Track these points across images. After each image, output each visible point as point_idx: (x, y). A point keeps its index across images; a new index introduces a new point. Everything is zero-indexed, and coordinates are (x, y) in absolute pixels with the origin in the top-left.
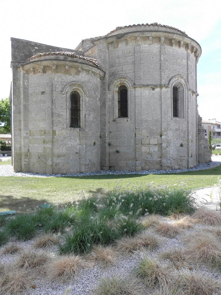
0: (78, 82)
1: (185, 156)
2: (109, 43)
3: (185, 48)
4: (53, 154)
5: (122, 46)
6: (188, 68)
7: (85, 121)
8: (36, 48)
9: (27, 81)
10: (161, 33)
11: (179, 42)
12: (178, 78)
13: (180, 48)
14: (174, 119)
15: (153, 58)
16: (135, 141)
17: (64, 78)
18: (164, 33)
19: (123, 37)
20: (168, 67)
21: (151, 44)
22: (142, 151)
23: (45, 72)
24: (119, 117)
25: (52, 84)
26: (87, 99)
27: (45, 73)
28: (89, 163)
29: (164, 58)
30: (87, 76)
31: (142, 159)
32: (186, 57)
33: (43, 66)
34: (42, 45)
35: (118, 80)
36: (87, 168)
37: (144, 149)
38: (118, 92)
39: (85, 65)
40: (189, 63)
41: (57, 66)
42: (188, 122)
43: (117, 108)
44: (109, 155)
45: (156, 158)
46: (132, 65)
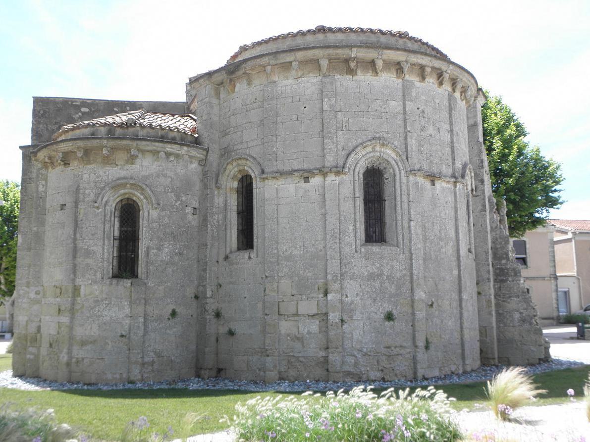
1: (405, 344)
3: (395, 74)
4: (71, 338)
5: (241, 87)
6: (405, 120)
7: (147, 262)
8: (83, 110)
9: (44, 182)
11: (373, 63)
12: (373, 148)
15: (305, 108)
16: (264, 307)
17: (101, 173)
18: (324, 50)
19: (238, 70)
21: (301, 77)
22: (280, 331)
24: (239, 249)
25: (78, 189)
26: (154, 214)
28: (156, 359)
29: (331, 106)
30: (156, 163)
31: (282, 353)
32: (400, 94)
33: (62, 153)
34: (97, 101)
35: (234, 164)
36: (148, 370)
37: (285, 327)
39: (144, 143)
40: (407, 106)
41: (87, 152)
42: (411, 254)
44: (217, 340)
45: (314, 350)
46: (259, 128)
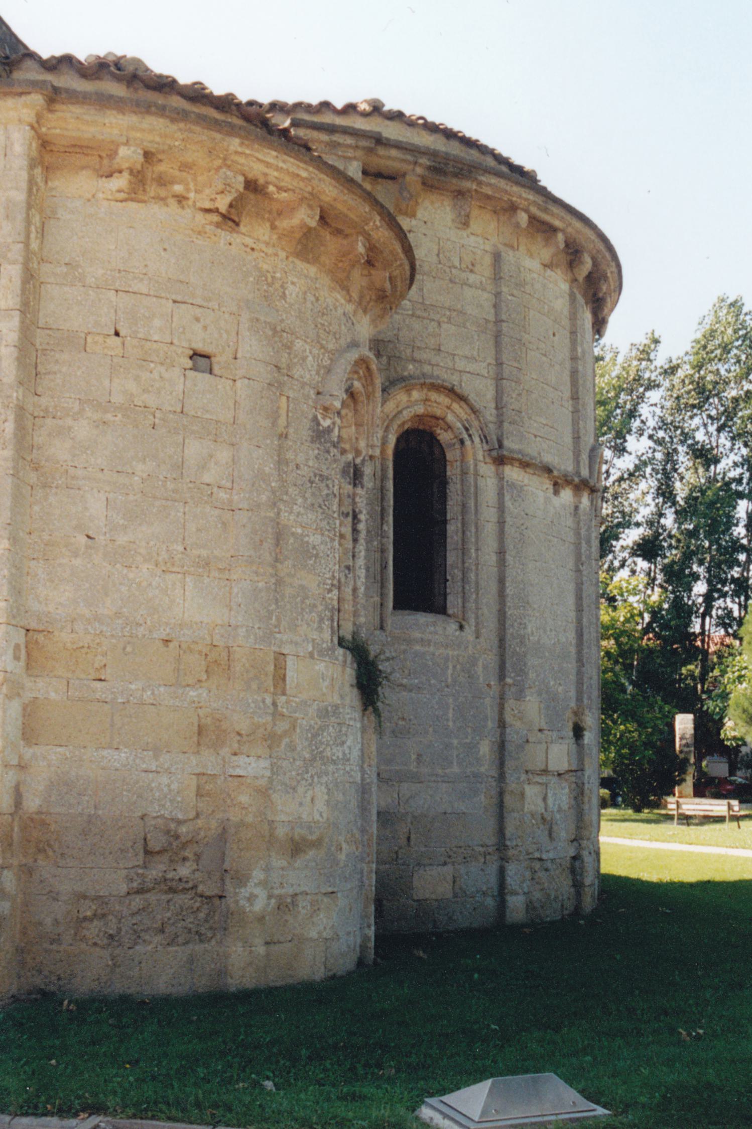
23: (234, 221)
27: (230, 223)
35: (415, 395)
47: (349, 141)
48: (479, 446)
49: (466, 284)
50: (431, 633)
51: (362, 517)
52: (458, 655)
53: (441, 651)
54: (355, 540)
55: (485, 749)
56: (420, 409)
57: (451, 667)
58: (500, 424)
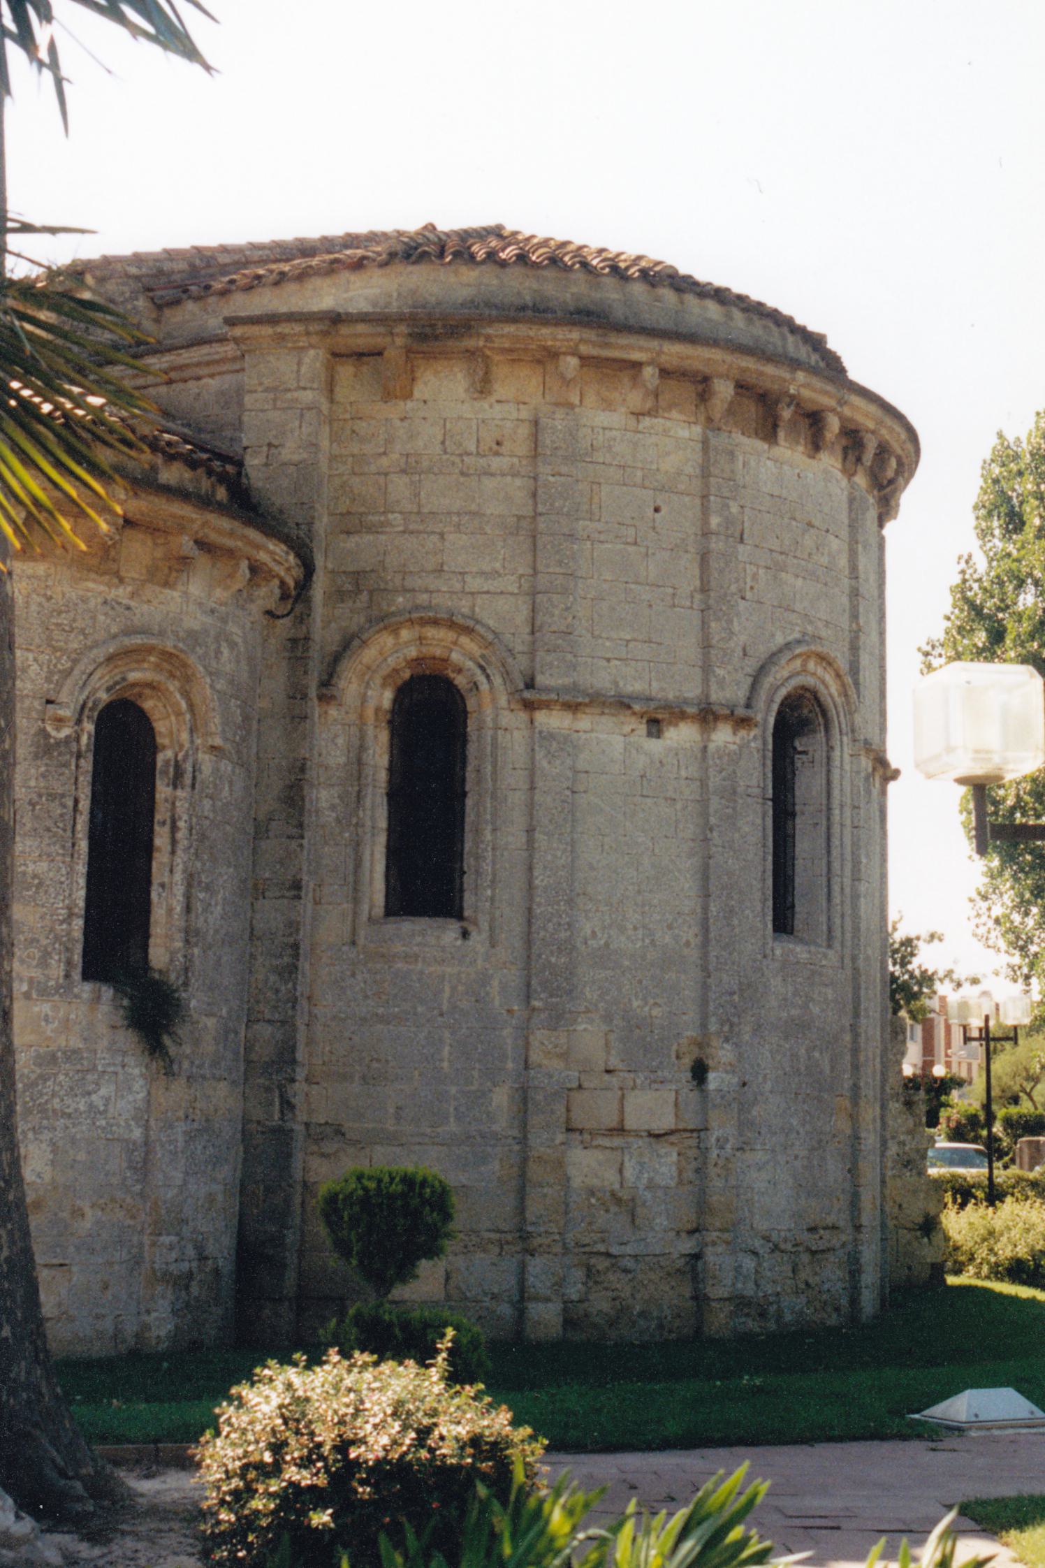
0: (162, 633)
1: (841, 1224)
2: (343, 351)
5: (444, 390)
10: (716, 354)
12: (804, 665)
13: (818, 456)
14: (780, 948)
15: (657, 510)
20: (748, 580)
35: (405, 634)
37: (588, 1166)
38: (390, 722)
43: (382, 839)
47: (298, 328)
48: (502, 688)
49: (486, 473)
50: (418, 945)
51: (181, 824)
52: (459, 973)
53: (432, 969)
54: (173, 852)
55: (501, 1098)
56: (412, 652)
57: (447, 989)
58: (532, 653)
